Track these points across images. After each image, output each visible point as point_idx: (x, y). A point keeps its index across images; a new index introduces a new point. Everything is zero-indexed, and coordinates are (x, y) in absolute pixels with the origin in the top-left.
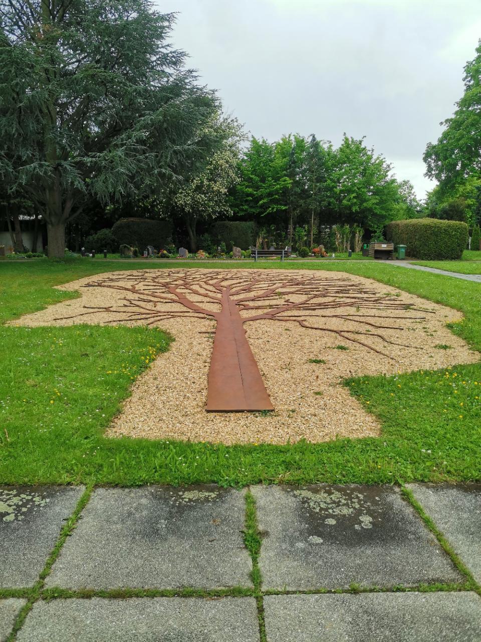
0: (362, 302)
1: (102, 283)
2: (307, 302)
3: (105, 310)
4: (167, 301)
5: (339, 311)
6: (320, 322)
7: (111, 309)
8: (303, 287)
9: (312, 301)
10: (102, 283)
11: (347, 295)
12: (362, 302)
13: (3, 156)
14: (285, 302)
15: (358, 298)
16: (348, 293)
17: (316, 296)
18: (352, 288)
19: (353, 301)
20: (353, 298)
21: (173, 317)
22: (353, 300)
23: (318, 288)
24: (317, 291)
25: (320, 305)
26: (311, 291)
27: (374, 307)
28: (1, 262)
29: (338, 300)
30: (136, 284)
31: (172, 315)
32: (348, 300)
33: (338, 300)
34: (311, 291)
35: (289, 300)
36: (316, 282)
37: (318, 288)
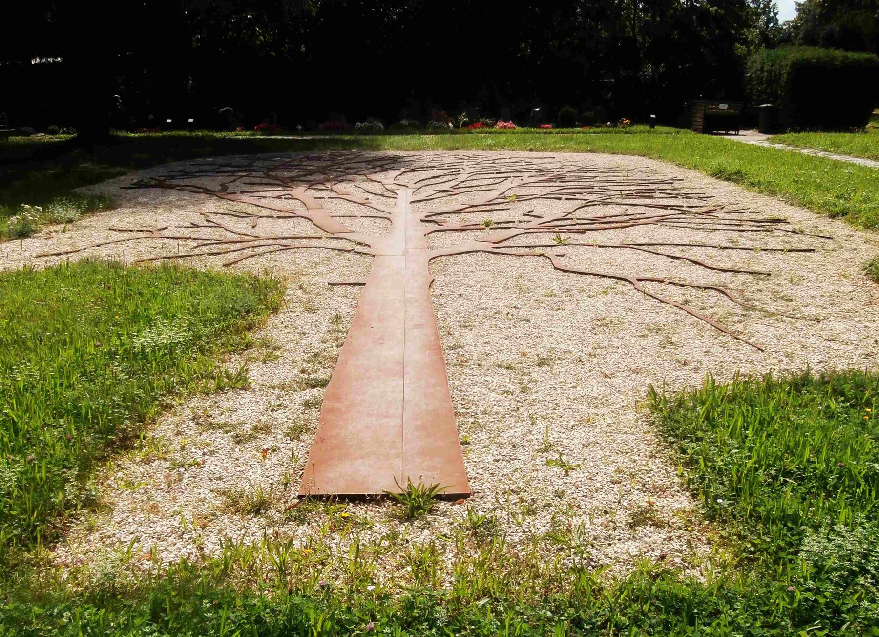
0: (679, 216)
1: (164, 181)
2: (569, 217)
3: (148, 234)
4: (282, 214)
5: (637, 234)
6: (598, 260)
7: (166, 233)
8: (562, 184)
9: (580, 214)
10: (164, 181)
11: (648, 201)
12: (679, 216)
13: (8, 449)
14: (524, 215)
15: (672, 207)
16: (652, 197)
17: (588, 204)
18: (661, 186)
19: (662, 214)
20: (665, 207)
21: (286, 248)
22: (663, 212)
23: (592, 188)
24: (589, 193)
25: (593, 221)
26: (578, 193)
27: (503, 200)
28: (877, 158)
29: (631, 210)
30: (231, 182)
31: (285, 244)
32: (651, 212)
33: (631, 210)
34: (578, 193)
35: (532, 211)
36: (589, 174)
37: (592, 188)
